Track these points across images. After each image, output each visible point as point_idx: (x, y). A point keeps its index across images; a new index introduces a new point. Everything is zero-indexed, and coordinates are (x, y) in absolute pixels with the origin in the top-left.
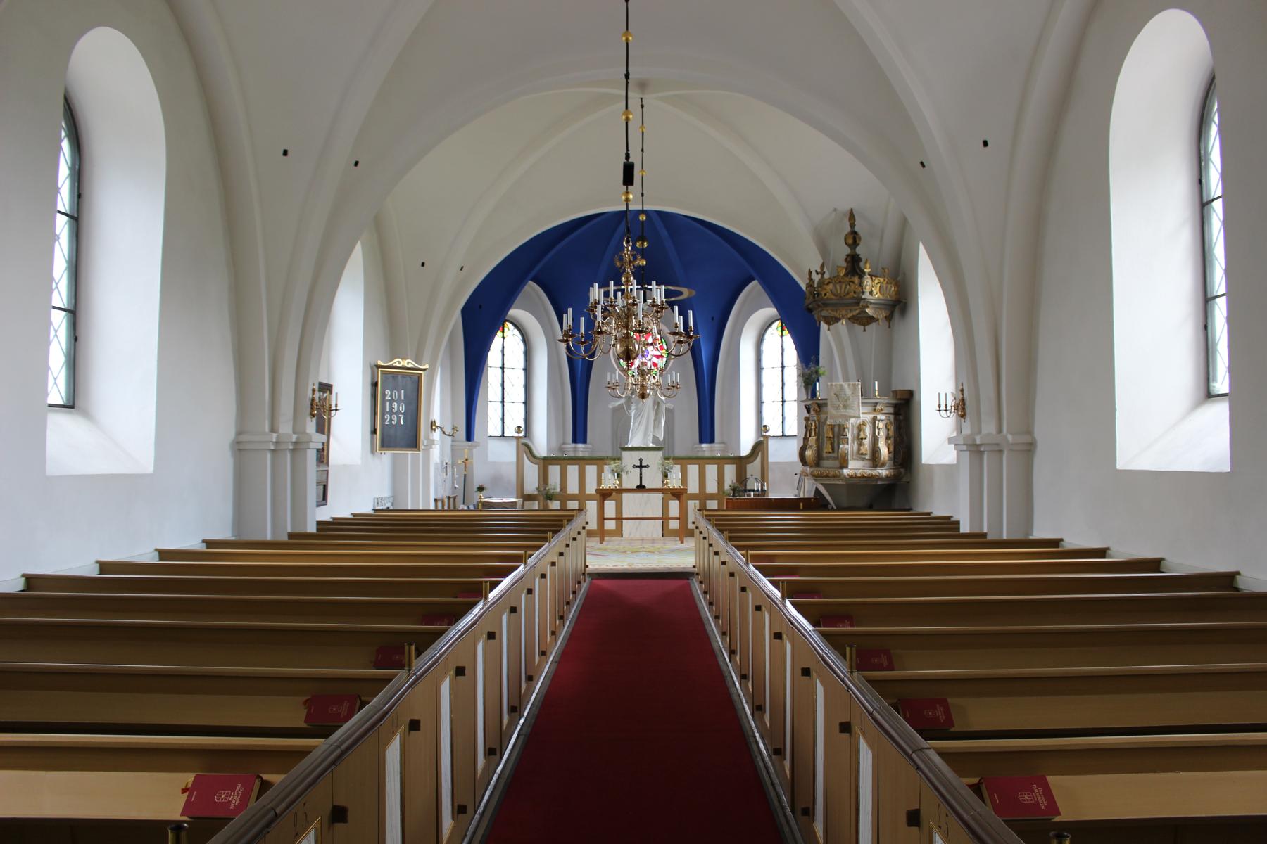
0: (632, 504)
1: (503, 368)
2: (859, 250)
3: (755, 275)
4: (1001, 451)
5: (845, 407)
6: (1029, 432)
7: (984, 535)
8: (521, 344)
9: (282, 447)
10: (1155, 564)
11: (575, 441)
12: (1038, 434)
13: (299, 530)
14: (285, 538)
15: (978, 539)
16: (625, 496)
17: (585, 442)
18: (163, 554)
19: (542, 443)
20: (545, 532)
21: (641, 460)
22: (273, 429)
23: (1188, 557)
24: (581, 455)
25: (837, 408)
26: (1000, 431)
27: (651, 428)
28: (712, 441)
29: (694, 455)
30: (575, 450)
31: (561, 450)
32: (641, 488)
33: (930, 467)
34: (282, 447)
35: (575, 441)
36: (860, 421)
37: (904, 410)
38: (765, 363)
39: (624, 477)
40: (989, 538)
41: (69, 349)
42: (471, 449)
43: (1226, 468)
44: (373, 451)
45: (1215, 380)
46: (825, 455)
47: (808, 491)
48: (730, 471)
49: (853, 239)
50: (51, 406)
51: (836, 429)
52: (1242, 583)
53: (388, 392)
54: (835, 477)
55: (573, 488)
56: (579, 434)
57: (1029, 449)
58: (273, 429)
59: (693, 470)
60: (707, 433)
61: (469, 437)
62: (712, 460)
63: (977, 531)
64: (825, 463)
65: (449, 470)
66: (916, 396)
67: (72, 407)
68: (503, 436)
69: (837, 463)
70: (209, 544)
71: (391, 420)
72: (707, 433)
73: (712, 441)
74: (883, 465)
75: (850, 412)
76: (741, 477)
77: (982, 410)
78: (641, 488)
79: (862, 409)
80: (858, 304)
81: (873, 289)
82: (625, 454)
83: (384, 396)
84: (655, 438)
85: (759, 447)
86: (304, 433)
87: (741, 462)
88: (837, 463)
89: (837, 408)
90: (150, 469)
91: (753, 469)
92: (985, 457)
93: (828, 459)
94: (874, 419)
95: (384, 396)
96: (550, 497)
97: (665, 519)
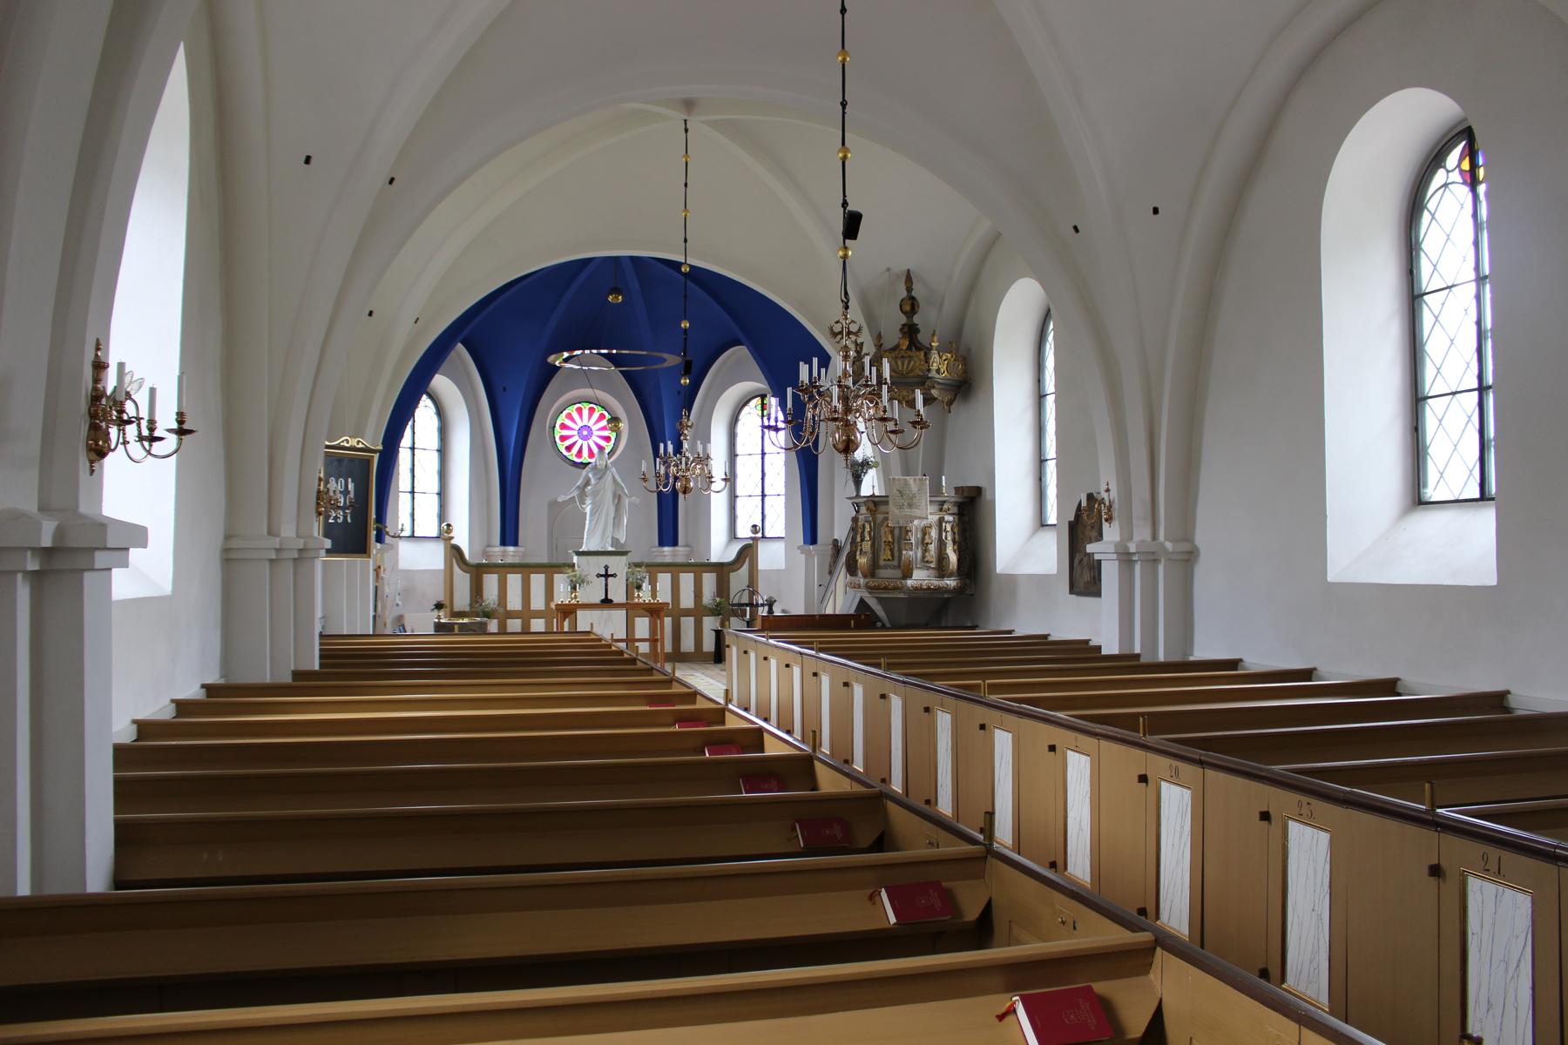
2: (916, 319)
3: (743, 338)
4: (1156, 561)
5: (910, 506)
7: (1138, 656)
10: (1390, 686)
11: (503, 543)
12: (1201, 539)
14: (288, 679)
15: (1127, 662)
17: (516, 544)
20: (878, 656)
21: (606, 568)
23: (1432, 677)
24: (509, 560)
26: (1154, 537)
27: (610, 528)
28: (675, 543)
30: (504, 554)
31: (485, 554)
32: (607, 602)
33: (1011, 579)
35: (503, 543)
36: (924, 522)
37: (971, 510)
38: (739, 449)
40: (1143, 660)
43: (1491, 580)
45: (1425, 486)
46: (882, 563)
47: (840, 601)
48: (709, 580)
49: (910, 306)
51: (896, 532)
52: (1513, 702)
54: (895, 589)
55: (514, 602)
56: (509, 535)
57: (1189, 558)
60: (668, 533)
62: (686, 567)
64: (882, 573)
66: (987, 495)
68: (413, 536)
69: (898, 573)
72: (668, 533)
73: (675, 543)
74: (950, 576)
75: (917, 512)
76: (722, 588)
77: (1135, 514)
78: (607, 602)
79: (930, 509)
81: (940, 366)
84: (615, 541)
85: (747, 553)
86: (311, 536)
87: (722, 570)
88: (898, 573)
91: (738, 580)
92: (1138, 568)
93: (886, 567)
94: (941, 520)
96: (715, 611)
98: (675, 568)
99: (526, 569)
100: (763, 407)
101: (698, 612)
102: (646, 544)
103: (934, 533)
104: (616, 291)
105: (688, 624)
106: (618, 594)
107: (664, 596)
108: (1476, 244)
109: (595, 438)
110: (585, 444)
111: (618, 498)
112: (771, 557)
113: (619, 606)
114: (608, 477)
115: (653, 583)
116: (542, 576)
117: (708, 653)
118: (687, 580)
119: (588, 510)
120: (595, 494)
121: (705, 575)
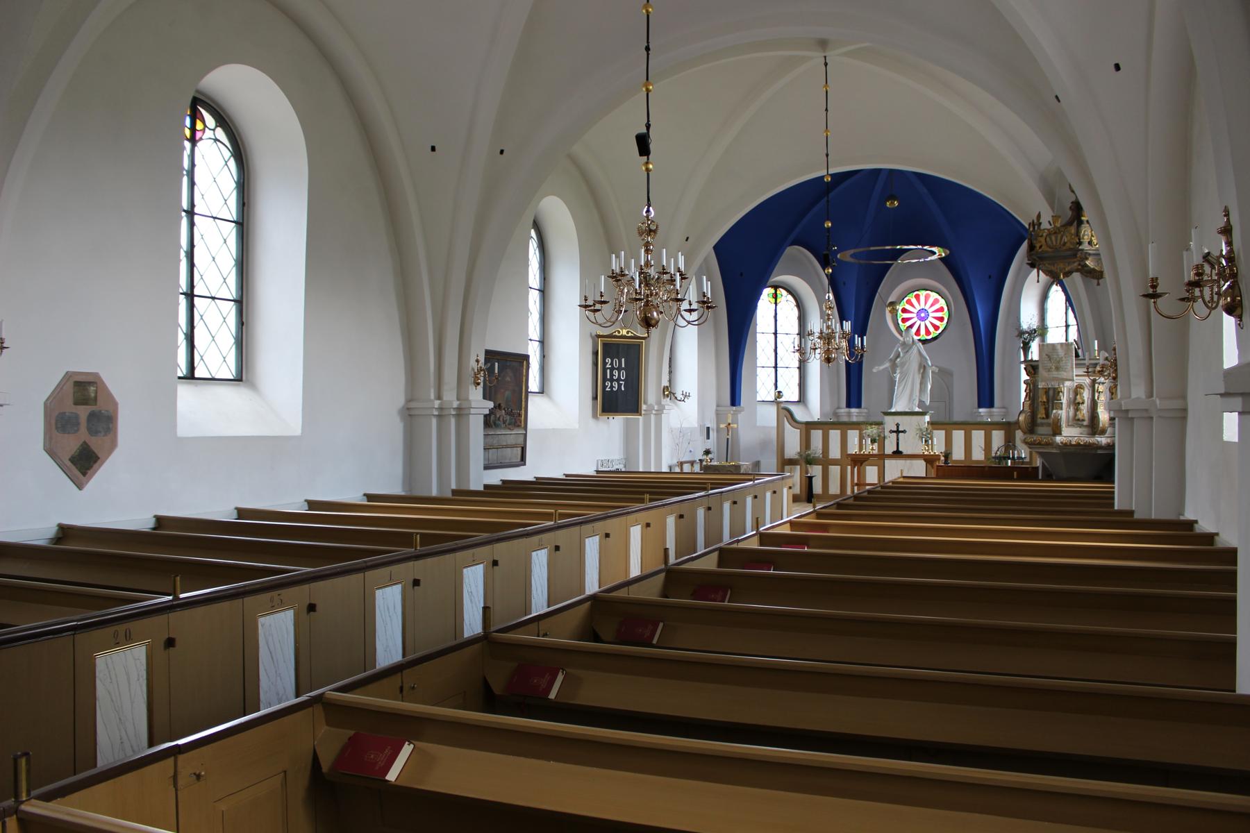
1: (775, 334)
5: (1057, 369)
6: (1184, 397)
7: (1131, 513)
8: (796, 310)
9: (445, 412)
11: (849, 405)
13: (464, 488)
14: (449, 495)
16: (887, 462)
17: (859, 406)
18: (312, 504)
19: (814, 410)
20: (643, 493)
21: (898, 425)
22: (439, 397)
24: (855, 419)
25: (1049, 370)
27: (917, 392)
28: (991, 405)
29: (970, 419)
30: (849, 414)
31: (836, 414)
34: (445, 412)
35: (849, 405)
40: (1136, 516)
41: (237, 332)
44: (595, 416)
46: (1039, 421)
51: (1051, 393)
53: (608, 360)
54: (1048, 444)
56: (854, 399)
57: (1181, 416)
58: (439, 397)
60: (986, 397)
61: (735, 400)
63: (408, 494)
64: (1041, 430)
65: (713, 434)
67: (241, 380)
70: (370, 497)
71: (612, 387)
72: (986, 397)
73: (991, 405)
74: (1103, 432)
75: (1064, 375)
78: (897, 454)
79: (1075, 372)
80: (1075, 256)
82: (888, 419)
83: (604, 363)
86: (467, 399)
89: (1049, 370)
90: (298, 431)
93: (1042, 425)
94: (1094, 382)
95: (604, 363)
96: (810, 461)
99: (988, 427)
103: (1086, 395)
104: (892, 198)
108: (193, 165)
109: (930, 319)
110: (923, 324)
111: (923, 368)
114: (914, 350)
120: (903, 364)
121: (994, 432)
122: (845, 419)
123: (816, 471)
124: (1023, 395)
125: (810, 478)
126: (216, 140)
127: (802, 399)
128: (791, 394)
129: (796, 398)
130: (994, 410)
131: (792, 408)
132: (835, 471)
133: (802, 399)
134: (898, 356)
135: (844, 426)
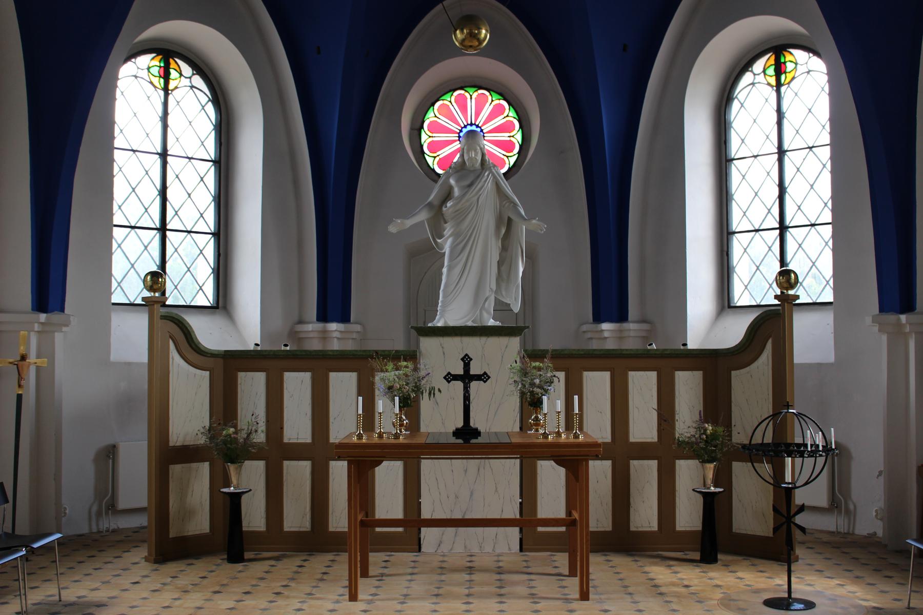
0: (447, 485)
11: (323, 317)
17: (344, 318)
19: (249, 326)
21: (467, 361)
24: (335, 346)
28: (621, 316)
30: (324, 336)
31: (294, 335)
35: (323, 317)
39: (425, 404)
42: (46, 332)
48: (688, 386)
50: (114, 304)
56: (334, 302)
59: (597, 383)
60: (610, 301)
62: (641, 359)
72: (610, 301)
73: (621, 316)
76: (716, 404)
82: (428, 345)
84: (501, 308)
87: (715, 365)
91: (751, 390)
96: (702, 450)
97: (527, 522)
98: (618, 362)
100: (780, 69)
101: (667, 450)
102: (567, 316)
105: (645, 473)
106: (497, 414)
107: (598, 428)
112: (811, 339)
113: (498, 449)
115: (574, 388)
116: (305, 378)
117: (687, 535)
118: (643, 385)
119: (447, 249)
120: (460, 216)
121: (335, 378)
122: (315, 345)
123: (250, 477)
124: (521, 269)
125: (236, 499)
126: (192, 87)
127: (223, 302)
128: (191, 284)
129: (205, 298)
130: (625, 325)
131: (195, 323)
132: (298, 473)
133: (223, 302)
134: (448, 195)
135: (321, 363)
